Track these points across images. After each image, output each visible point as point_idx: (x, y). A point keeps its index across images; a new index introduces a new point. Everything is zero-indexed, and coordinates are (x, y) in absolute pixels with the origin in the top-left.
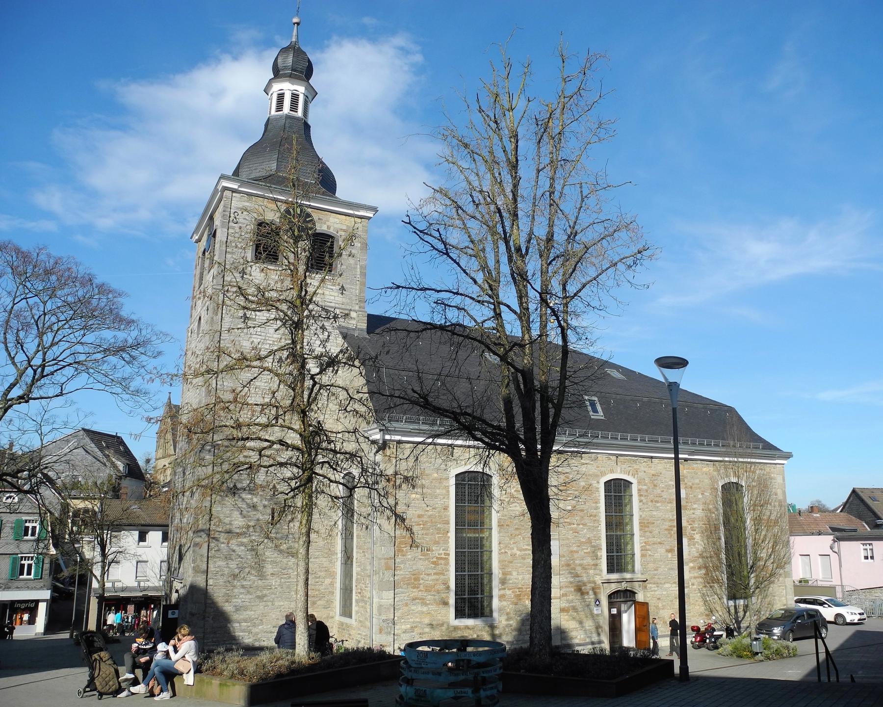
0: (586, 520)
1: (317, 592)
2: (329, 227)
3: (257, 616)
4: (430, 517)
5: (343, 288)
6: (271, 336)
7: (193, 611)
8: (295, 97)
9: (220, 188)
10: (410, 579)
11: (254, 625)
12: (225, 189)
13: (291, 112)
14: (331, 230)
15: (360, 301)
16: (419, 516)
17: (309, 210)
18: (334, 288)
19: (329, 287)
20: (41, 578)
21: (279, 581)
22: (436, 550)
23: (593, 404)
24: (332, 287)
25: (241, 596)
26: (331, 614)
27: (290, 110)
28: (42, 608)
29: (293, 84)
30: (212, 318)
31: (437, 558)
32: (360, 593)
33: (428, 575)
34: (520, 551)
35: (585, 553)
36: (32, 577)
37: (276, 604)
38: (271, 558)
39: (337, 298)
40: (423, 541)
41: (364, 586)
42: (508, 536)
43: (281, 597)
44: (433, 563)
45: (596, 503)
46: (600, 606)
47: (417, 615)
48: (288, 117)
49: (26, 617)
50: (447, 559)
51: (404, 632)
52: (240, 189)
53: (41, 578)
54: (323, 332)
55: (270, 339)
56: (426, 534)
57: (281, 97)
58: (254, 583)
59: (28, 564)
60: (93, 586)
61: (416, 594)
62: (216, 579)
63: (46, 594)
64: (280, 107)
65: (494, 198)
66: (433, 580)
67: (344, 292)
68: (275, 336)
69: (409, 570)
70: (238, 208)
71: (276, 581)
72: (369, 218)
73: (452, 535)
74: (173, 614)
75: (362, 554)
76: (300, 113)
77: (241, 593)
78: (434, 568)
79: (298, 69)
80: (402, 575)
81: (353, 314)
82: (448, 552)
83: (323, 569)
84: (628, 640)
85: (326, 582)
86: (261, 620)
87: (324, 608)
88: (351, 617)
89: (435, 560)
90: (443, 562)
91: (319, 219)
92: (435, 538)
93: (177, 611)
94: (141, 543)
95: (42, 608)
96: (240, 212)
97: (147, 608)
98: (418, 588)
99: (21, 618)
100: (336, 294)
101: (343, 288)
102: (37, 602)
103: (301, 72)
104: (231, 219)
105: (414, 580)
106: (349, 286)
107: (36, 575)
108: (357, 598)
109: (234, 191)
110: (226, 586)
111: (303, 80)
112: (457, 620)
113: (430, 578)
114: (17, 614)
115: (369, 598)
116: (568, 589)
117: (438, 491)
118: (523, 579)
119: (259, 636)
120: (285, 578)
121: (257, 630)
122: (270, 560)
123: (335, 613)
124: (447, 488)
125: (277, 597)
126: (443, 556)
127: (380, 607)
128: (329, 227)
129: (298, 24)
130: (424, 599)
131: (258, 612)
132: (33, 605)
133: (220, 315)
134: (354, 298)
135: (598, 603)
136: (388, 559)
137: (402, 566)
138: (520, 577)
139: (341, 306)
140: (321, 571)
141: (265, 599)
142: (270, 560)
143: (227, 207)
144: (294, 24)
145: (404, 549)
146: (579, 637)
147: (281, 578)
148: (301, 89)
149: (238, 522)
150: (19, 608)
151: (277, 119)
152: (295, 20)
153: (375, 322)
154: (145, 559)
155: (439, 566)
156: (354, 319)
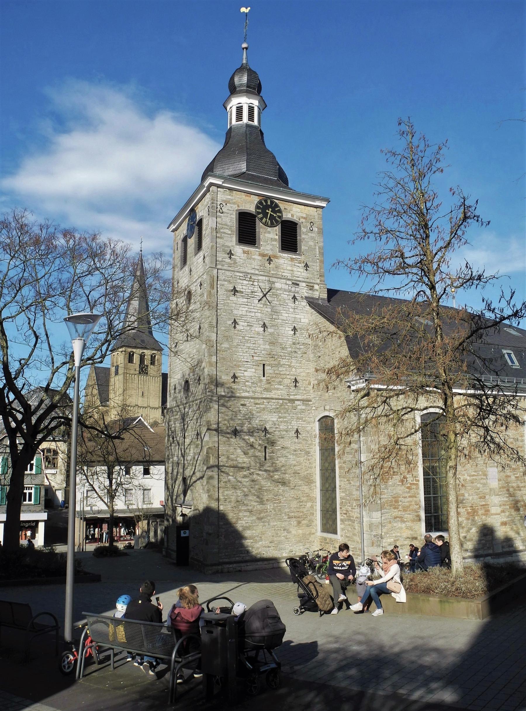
1: (302, 514)
2: (292, 216)
3: (257, 534)
5: (306, 266)
7: (210, 532)
8: (251, 110)
9: (206, 184)
10: (391, 501)
12: (211, 184)
13: (249, 122)
14: (295, 218)
15: (320, 276)
17: (277, 201)
18: (300, 265)
19: (296, 264)
20: (39, 504)
21: (272, 505)
23: (509, 355)
24: (299, 265)
25: (244, 519)
26: (313, 531)
28: (41, 527)
29: (249, 98)
30: (210, 292)
31: (411, 484)
32: (345, 514)
33: (405, 497)
34: (470, 476)
36: (32, 502)
37: (272, 524)
38: (266, 487)
41: (350, 508)
43: (275, 518)
44: (408, 488)
45: (522, 436)
47: (398, 530)
48: (247, 126)
49: (29, 533)
50: (417, 484)
51: (389, 545)
52: (223, 185)
53: (39, 504)
54: (294, 301)
57: (239, 110)
58: (254, 507)
59: (29, 493)
60: (77, 510)
61: (397, 513)
63: (44, 516)
64: (239, 116)
66: (408, 502)
67: (308, 269)
68: (259, 305)
70: (223, 201)
72: (323, 207)
74: (185, 533)
76: (256, 123)
77: (245, 516)
78: (409, 492)
80: (386, 498)
81: (316, 287)
85: (308, 505)
86: (261, 537)
87: (307, 526)
88: (335, 532)
89: (409, 485)
90: (414, 487)
91: (285, 209)
93: (187, 531)
94: (145, 476)
95: (41, 527)
96: (224, 204)
97: (117, 526)
98: (398, 508)
99: (26, 534)
100: (302, 270)
101: (306, 266)
102: (37, 522)
103: (254, 89)
104: (218, 210)
105: (395, 503)
107: (36, 500)
108: (343, 518)
109: (219, 186)
111: (256, 95)
113: (406, 500)
114: (22, 531)
116: (505, 507)
118: (473, 499)
121: (258, 546)
123: (316, 530)
125: (272, 519)
127: (371, 526)
128: (292, 216)
129: (247, 48)
130: (402, 517)
131: (258, 531)
132: (34, 524)
133: (215, 288)
134: (316, 273)
137: (386, 491)
138: (471, 498)
139: (306, 280)
140: (303, 497)
141: (263, 520)
143: (214, 200)
144: (243, 49)
147: (275, 503)
148: (255, 103)
149: (243, 459)
150: (24, 527)
151: (239, 127)
152: (244, 45)
153: (332, 293)
154: (149, 488)
155: (412, 490)
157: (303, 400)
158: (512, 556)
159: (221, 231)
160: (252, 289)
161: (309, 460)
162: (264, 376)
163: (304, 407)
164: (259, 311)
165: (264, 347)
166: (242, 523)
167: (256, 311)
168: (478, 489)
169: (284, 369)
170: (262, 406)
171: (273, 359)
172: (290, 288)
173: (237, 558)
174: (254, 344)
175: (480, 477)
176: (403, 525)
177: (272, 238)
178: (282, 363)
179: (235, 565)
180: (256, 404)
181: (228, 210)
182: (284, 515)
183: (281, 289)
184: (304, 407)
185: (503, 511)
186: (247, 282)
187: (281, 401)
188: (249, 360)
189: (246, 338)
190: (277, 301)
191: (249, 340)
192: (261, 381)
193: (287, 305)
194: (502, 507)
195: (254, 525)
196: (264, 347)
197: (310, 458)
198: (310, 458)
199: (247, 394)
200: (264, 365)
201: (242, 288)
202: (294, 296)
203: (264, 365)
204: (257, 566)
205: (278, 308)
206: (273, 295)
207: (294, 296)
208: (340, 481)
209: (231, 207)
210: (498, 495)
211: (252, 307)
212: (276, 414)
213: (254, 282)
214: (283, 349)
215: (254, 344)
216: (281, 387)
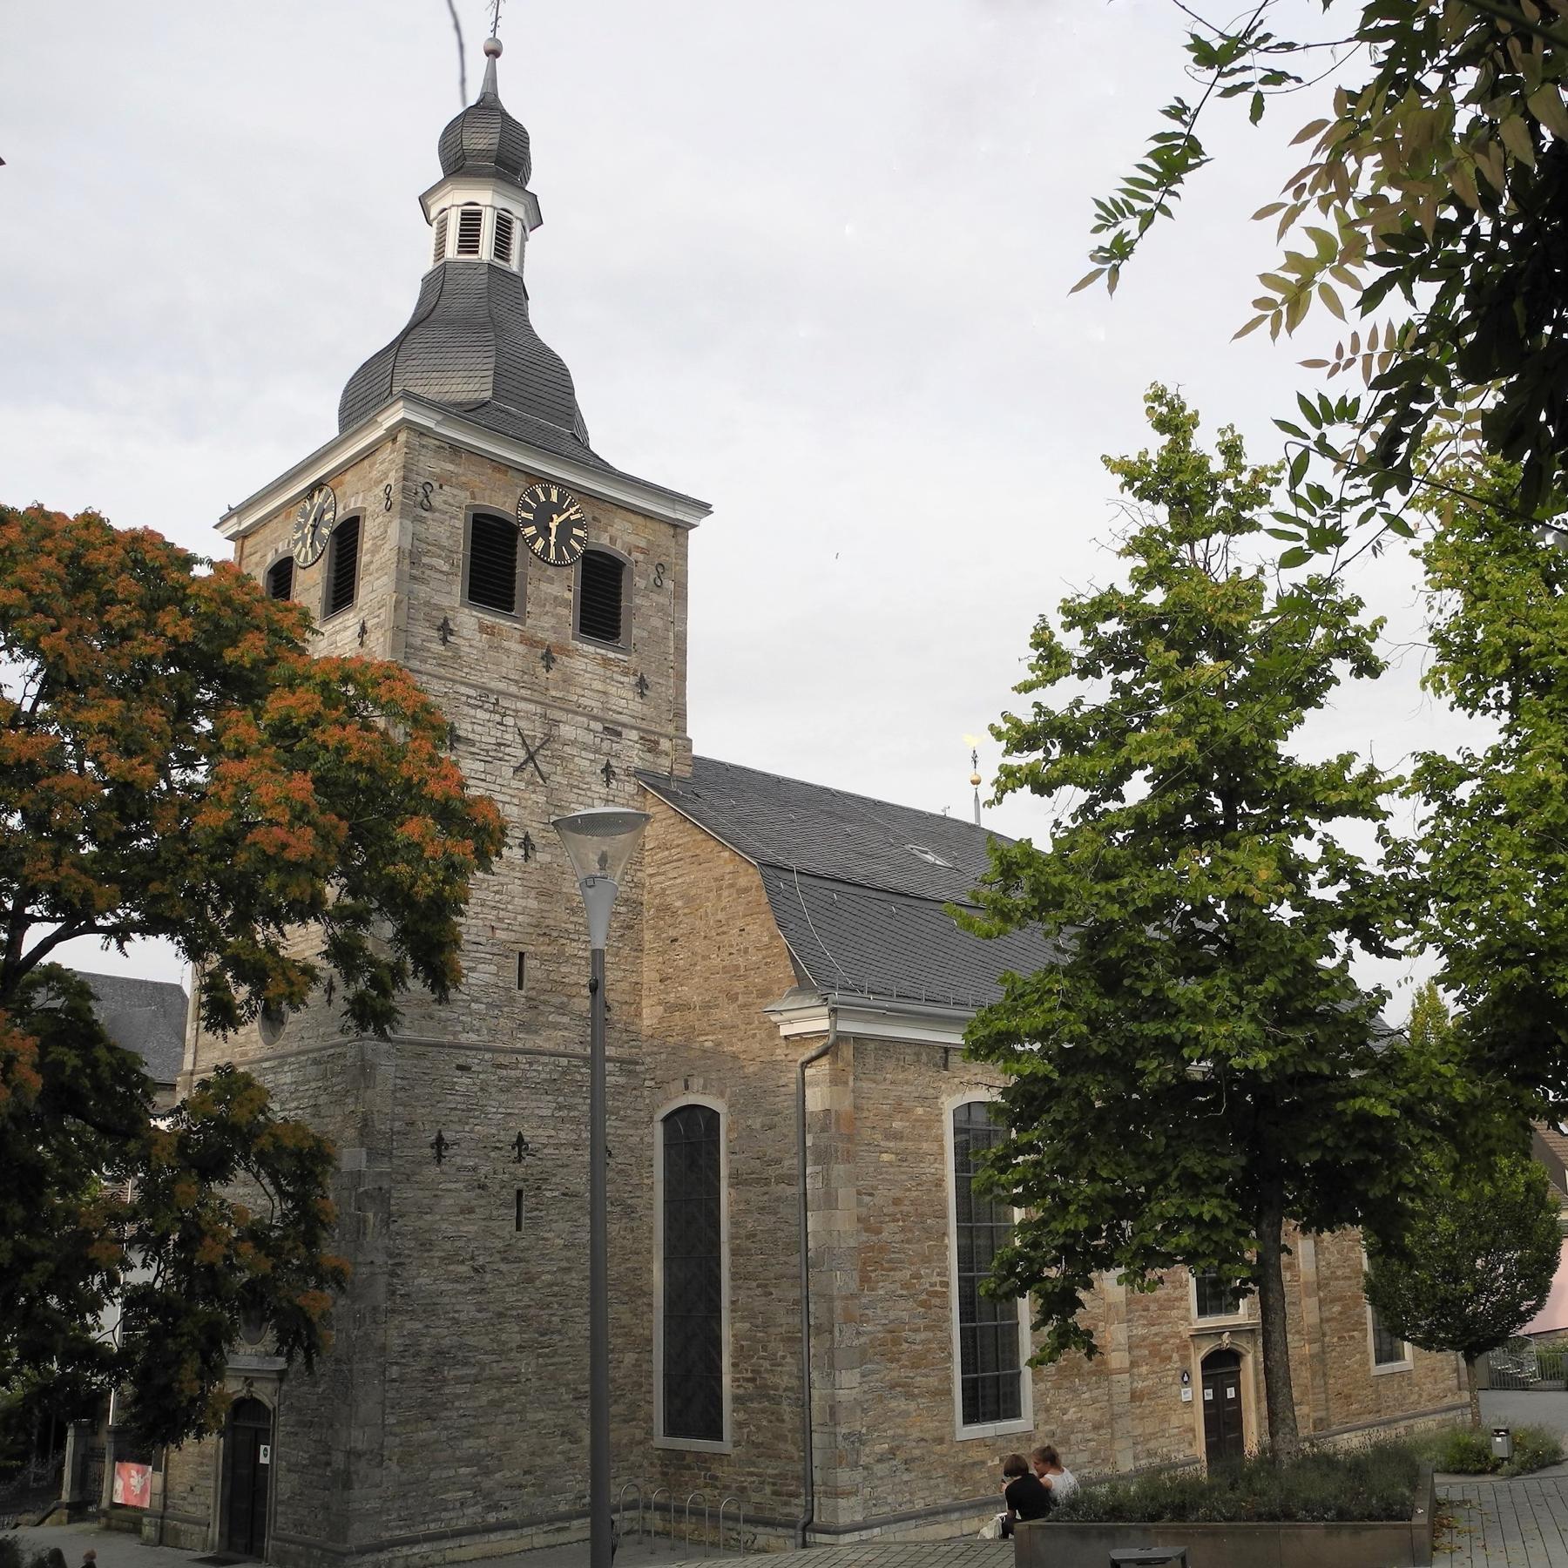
4: (913, 1203)
5: (642, 684)
6: (505, 783)
11: (487, 1472)
13: (497, 260)
14: (618, 547)
16: (897, 1202)
25: (457, 1404)
39: (632, 705)
40: (903, 1256)
44: (923, 1304)
46: (1191, 1386)
51: (879, 1461)
55: (504, 790)
56: (909, 1241)
61: (895, 1374)
62: (404, 1365)
66: (923, 1342)
68: (514, 784)
69: (883, 1322)
73: (952, 1241)
75: (759, 1291)
77: (458, 1397)
79: (510, 162)
80: (870, 1333)
82: (945, 1279)
83: (619, 1331)
85: (627, 1360)
87: (625, 1421)
89: (924, 1297)
91: (594, 519)
96: (436, 485)
98: (898, 1360)
100: (630, 695)
106: (656, 680)
108: (741, 1391)
110: (427, 1381)
112: (968, 1428)
117: (925, 1145)
119: (496, 1497)
120: (547, 1355)
124: (939, 1140)
126: (938, 1288)
128: (613, 540)
131: (494, 1440)
134: (664, 707)
135: (1186, 1379)
136: (847, 1298)
139: (639, 723)
141: (507, 1406)
142: (515, 1313)
145: (873, 1275)
147: (539, 1355)
156: (667, 754)
157: (622, 1062)
160: (499, 735)
161: (632, 1230)
162: (520, 987)
163: (622, 1080)
164: (516, 801)
165: (523, 903)
166: (449, 1418)
169: (574, 970)
170: (518, 1073)
171: (547, 940)
172: (598, 740)
173: (432, 1526)
174: (496, 892)
176: (912, 1406)
178: (569, 951)
179: (425, 1548)
180: (500, 1066)
182: (563, 1390)
183: (573, 743)
184: (622, 1080)
186: (487, 716)
187: (564, 1061)
188: (483, 940)
190: (563, 775)
192: (512, 1000)
193: (589, 789)
195: (481, 1420)
196: (523, 903)
197: (635, 1224)
198: (635, 1224)
199: (473, 1037)
200: (522, 955)
201: (473, 731)
202: (608, 765)
203: (522, 955)
204: (488, 1547)
205: (565, 796)
206: (553, 757)
207: (608, 765)
208: (735, 1288)
211: (498, 788)
212: (549, 1098)
213: (504, 715)
214: (573, 911)
215: (496, 892)
216: (565, 1020)
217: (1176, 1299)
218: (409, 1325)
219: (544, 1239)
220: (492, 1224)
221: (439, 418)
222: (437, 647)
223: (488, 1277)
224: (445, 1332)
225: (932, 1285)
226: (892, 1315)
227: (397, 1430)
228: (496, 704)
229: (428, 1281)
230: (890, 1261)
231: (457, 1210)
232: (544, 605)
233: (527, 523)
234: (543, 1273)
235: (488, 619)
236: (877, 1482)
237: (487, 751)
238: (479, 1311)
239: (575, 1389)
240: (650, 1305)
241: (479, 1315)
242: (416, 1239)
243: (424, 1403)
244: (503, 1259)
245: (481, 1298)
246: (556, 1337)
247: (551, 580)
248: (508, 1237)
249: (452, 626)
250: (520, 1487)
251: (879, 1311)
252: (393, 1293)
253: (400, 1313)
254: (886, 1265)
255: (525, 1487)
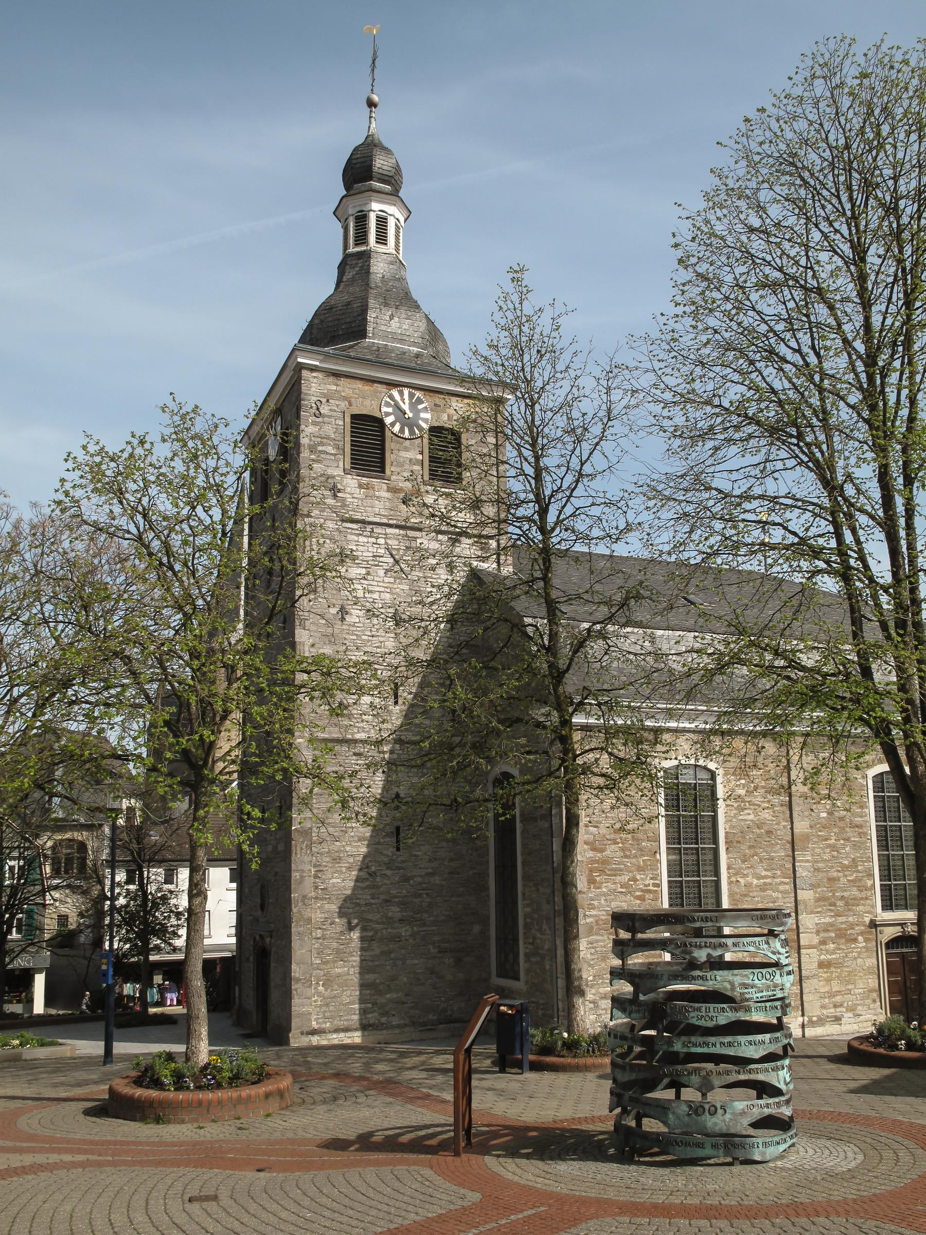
0: (849, 832)
6: (381, 579)
9: (292, 365)
22: (642, 879)
27: (377, 242)
35: (848, 881)
42: (739, 858)
45: (862, 807)
65: (913, 290)
68: (386, 580)
71: (406, 931)
84: (452, 1128)
88: (517, 978)
92: (639, 862)
96: (324, 400)
108: (528, 951)
115: (548, 950)
121: (383, 1001)
122: (396, 900)
126: (651, 888)
141: (392, 956)
145: (598, 879)
146: (845, 1005)
158: (840, 1024)
159: (320, 448)
162: (396, 703)
167: (382, 589)
168: (775, 902)
174: (377, 647)
175: (778, 880)
177: (411, 460)
181: (331, 410)
182: (431, 947)
185: (823, 942)
186: (365, 540)
189: (364, 637)
191: (369, 641)
194: (822, 935)
208: (524, 886)
209: (337, 406)
210: (812, 913)
211: (376, 583)
213: (377, 538)
215: (377, 647)
217: (862, 899)
218: (327, 906)
219: (415, 856)
220: (379, 847)
221: (321, 357)
222: (330, 501)
223: (378, 879)
224: (351, 910)
225: (646, 886)
226: (614, 905)
227: (322, 967)
228: (372, 531)
229: (339, 881)
230: (612, 870)
231: (356, 839)
232: (403, 466)
233: (388, 414)
234: (415, 876)
235: (365, 480)
236: (601, 1012)
237: (367, 561)
238: (372, 898)
239: (439, 947)
240: (488, 896)
241: (373, 901)
242: (330, 856)
243: (338, 951)
244: (388, 868)
245: (373, 891)
246: (425, 915)
247: (406, 449)
248: (390, 854)
249: (339, 486)
250: (403, 1003)
251: (603, 902)
252: (316, 888)
253: (322, 899)
254: (608, 872)
255: (407, 1003)
